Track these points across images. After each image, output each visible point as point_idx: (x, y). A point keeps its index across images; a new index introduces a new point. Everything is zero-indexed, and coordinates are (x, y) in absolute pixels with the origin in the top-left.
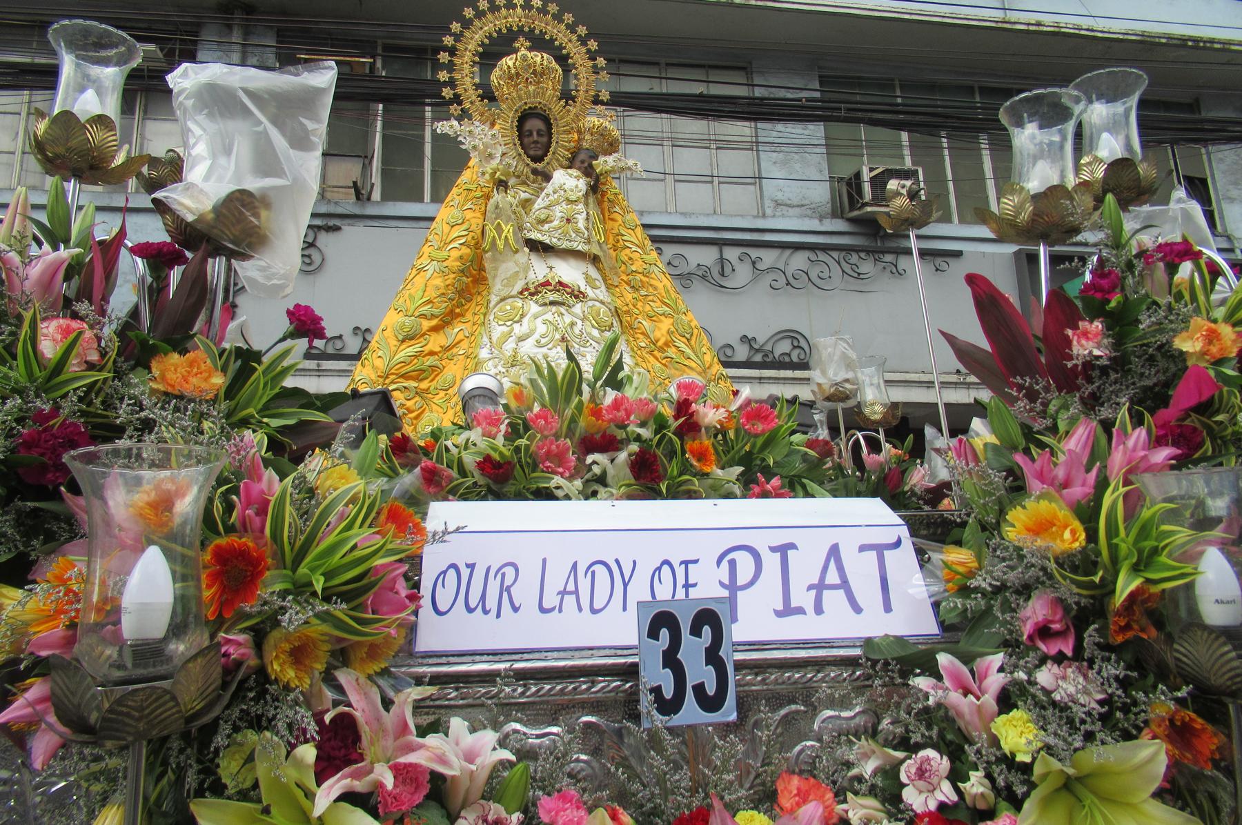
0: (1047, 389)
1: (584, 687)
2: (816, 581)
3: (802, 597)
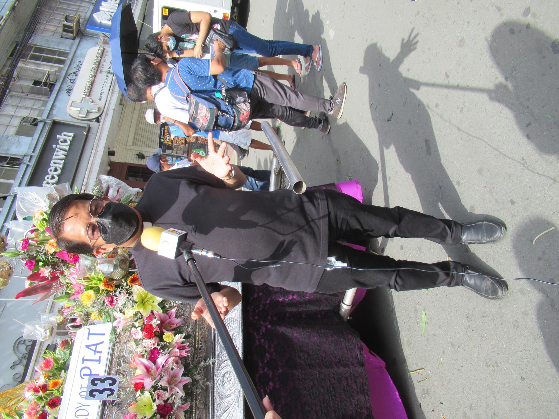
1: (106, 417)
3: (96, 357)
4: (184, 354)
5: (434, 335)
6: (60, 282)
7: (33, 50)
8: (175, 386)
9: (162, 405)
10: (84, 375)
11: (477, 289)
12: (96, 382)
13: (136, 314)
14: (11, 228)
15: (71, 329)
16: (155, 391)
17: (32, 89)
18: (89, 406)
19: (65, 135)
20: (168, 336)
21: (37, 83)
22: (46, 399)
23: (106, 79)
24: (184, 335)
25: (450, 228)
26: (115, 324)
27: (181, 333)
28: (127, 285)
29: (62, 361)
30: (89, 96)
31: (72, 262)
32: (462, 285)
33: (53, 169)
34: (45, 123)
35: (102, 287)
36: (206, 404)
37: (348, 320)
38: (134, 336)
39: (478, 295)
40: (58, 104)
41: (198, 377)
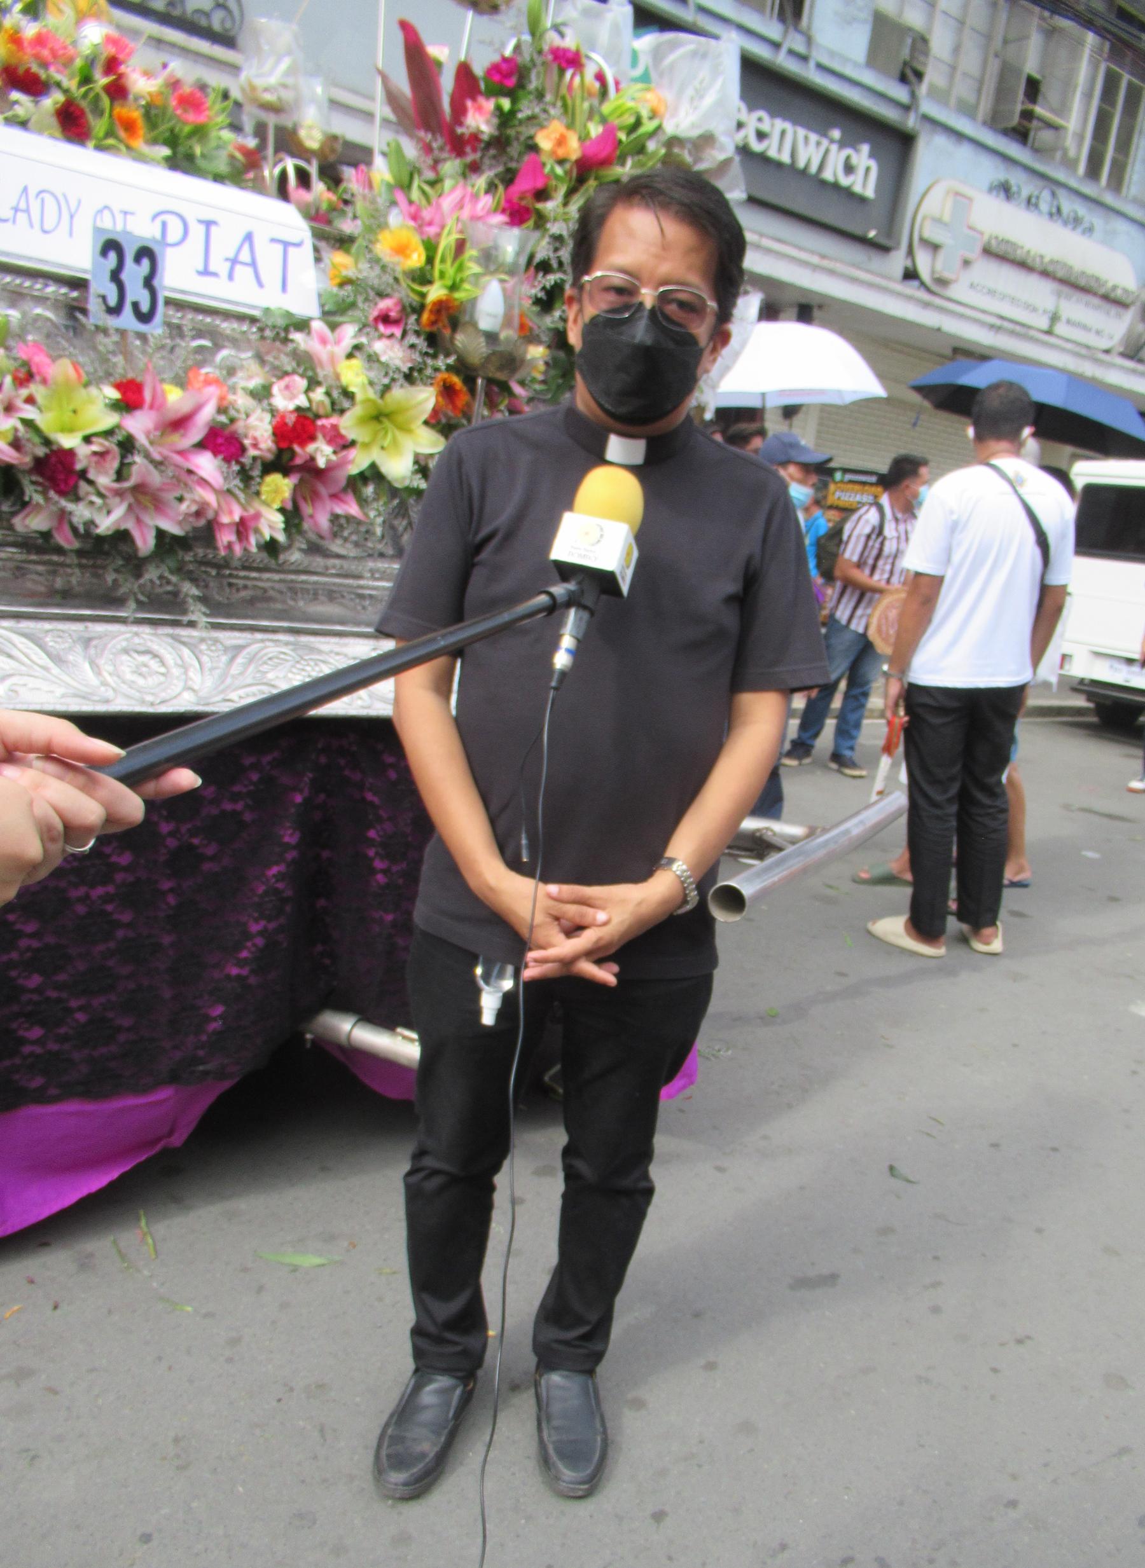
0: (441, 149)
2: (231, 255)
3: (218, 264)
4: (225, 537)
5: (261, 1289)
6: (445, 160)
7: (1135, 81)
8: (130, 507)
9: (73, 463)
10: (164, 225)
11: (405, 1411)
12: (146, 263)
13: (348, 395)
14: (610, 10)
15: (277, 171)
16: (120, 444)
17: (1018, 71)
18: (71, 234)
19: (868, 170)
20: (280, 486)
21: (1033, 88)
22: (85, 96)
23: (1035, 310)
24: (281, 537)
25: (586, 1337)
26: (317, 325)
27: (287, 530)
28: (437, 370)
29: (198, 150)
30: (987, 252)
31: (509, 201)
32: (416, 1371)
33: (765, 127)
34: (906, 108)
35: (435, 293)
36: (66, 596)
37: (302, 1034)
38: (283, 383)
39: (384, 1418)
40: (965, 151)
41: (152, 574)
